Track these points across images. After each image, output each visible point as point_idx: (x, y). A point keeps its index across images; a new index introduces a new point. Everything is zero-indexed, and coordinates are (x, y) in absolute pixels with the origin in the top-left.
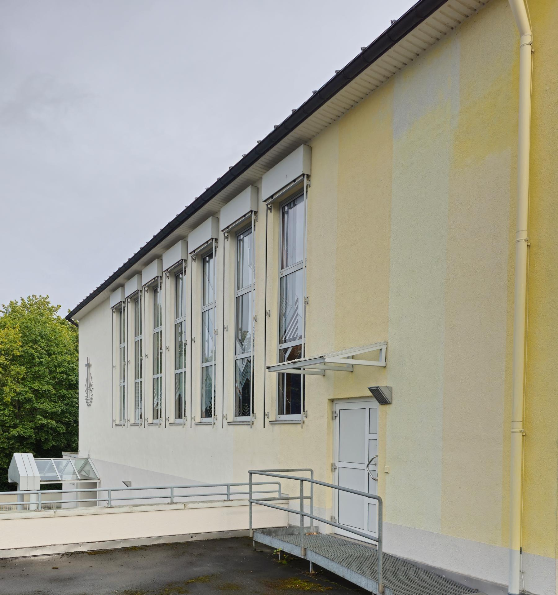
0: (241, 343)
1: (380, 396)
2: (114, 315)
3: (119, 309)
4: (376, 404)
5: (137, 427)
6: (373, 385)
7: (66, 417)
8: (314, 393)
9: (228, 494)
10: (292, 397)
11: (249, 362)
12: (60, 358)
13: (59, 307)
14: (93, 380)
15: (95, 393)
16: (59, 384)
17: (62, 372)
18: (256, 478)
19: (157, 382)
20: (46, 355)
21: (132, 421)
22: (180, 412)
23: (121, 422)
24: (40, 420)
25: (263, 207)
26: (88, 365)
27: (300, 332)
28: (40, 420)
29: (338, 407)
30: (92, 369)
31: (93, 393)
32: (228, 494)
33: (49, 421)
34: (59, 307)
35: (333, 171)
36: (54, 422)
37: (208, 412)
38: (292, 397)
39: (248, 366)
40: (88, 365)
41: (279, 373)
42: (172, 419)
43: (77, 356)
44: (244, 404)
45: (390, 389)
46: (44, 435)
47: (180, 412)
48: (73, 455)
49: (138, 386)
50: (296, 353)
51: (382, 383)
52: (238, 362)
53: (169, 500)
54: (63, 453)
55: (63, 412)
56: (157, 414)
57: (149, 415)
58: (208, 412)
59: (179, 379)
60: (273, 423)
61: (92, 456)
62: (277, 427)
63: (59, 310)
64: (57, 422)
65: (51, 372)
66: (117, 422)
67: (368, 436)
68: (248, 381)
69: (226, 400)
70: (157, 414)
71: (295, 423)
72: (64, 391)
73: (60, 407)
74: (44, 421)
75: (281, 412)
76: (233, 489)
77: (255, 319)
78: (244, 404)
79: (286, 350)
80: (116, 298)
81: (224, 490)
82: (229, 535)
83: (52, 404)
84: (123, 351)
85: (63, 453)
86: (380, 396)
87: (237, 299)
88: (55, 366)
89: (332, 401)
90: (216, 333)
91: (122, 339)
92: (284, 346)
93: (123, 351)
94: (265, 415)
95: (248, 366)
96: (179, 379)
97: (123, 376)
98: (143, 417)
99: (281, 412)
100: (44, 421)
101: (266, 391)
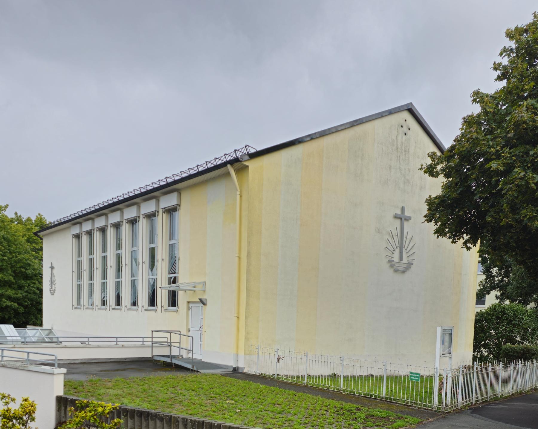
0: (152, 271)
1: (203, 302)
2: (74, 239)
3: (78, 237)
4: (202, 305)
5: (79, 310)
6: (201, 297)
7: (26, 302)
8: (182, 298)
9: (143, 342)
10: (173, 300)
11: (155, 281)
12: (20, 257)
13: (7, 206)
14: (56, 278)
15: (58, 286)
16: (16, 275)
17: (22, 267)
18: (155, 334)
19: (104, 285)
21: (87, 306)
22: (118, 302)
24: (5, 302)
25: (161, 211)
26: (52, 268)
28: (5, 302)
29: (191, 305)
30: (55, 271)
31: (56, 286)
32: (143, 342)
33: (12, 303)
34: (7, 206)
35: (190, 204)
36: (16, 304)
37: (134, 304)
38: (173, 300)
39: (154, 282)
40: (52, 268)
42: (114, 306)
44: (152, 301)
45: (206, 300)
46: (7, 314)
47: (118, 302)
48: (39, 328)
49: (91, 286)
50: (175, 281)
51: (203, 297)
52: (150, 280)
53: (119, 339)
54: (27, 326)
55: (24, 298)
56: (104, 303)
57: (98, 302)
58: (134, 304)
59: (118, 285)
61: (54, 328)
62: (167, 313)
63: (7, 209)
64: (19, 304)
65: (12, 267)
66: (76, 306)
68: (154, 290)
70: (104, 303)
71: (174, 311)
72: (23, 281)
73: (21, 293)
74: (9, 303)
75: (169, 306)
78: (152, 301)
79: (171, 278)
80: (76, 230)
81: (141, 339)
82: (143, 359)
83: (13, 292)
84: (79, 263)
85: (27, 326)
86: (203, 302)
88: (15, 262)
89: (189, 302)
91: (79, 255)
93: (79, 263)
94: (162, 307)
95: (154, 282)
96: (118, 285)
97: (79, 277)
98: (94, 304)
99: (169, 306)
100: (9, 303)
101: (162, 297)
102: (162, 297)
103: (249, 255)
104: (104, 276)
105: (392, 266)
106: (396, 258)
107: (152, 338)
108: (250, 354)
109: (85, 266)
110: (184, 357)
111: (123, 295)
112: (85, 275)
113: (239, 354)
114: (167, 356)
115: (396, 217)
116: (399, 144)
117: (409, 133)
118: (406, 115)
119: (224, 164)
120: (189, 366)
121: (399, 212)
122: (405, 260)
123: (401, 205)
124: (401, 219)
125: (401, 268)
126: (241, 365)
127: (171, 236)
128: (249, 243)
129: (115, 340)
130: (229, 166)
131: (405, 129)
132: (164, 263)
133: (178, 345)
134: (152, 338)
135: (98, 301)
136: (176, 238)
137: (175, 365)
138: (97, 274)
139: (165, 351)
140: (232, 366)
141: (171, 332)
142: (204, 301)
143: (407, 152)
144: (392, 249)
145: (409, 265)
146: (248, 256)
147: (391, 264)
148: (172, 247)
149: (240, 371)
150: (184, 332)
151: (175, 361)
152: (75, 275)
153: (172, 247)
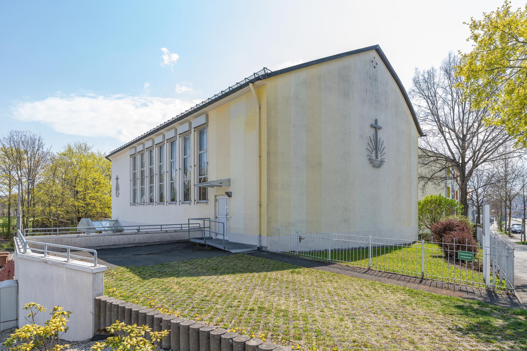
1: (229, 195)
4: (228, 197)
8: (211, 193)
15: (121, 191)
20: (458, 137)
23: (134, 202)
27: (206, 173)
30: (119, 180)
41: (200, 188)
43: (299, 252)
51: (229, 190)
60: (198, 203)
67: (226, 207)
69: (180, 195)
76: (183, 226)
77: (191, 167)
81: (180, 226)
87: (184, 159)
90: (176, 170)
92: (201, 177)
93: (134, 174)
95: (188, 183)
97: (135, 184)
99: (200, 199)
101: (194, 193)
102: (194, 193)
103: (268, 153)
104: (151, 182)
105: (371, 163)
106: (374, 157)
107: (189, 224)
108: (271, 236)
109: (138, 176)
110: (214, 238)
111: (165, 194)
112: (139, 182)
113: (262, 235)
114: (202, 239)
115: (372, 126)
116: (371, 74)
117: (377, 66)
118: (374, 53)
119: (247, 84)
120: (221, 247)
121: (373, 123)
122: (379, 159)
123: (374, 119)
124: (376, 128)
125: (377, 163)
126: (264, 244)
127: (201, 147)
128: (268, 144)
129: (160, 227)
130: (250, 84)
131: (374, 63)
132: (196, 168)
133: (208, 229)
134: (189, 224)
135: (147, 197)
136: (205, 148)
137: (209, 246)
138: (147, 181)
139: (199, 235)
140: (256, 246)
141: (204, 219)
142: (230, 194)
143: (376, 80)
144: (371, 150)
145: (382, 162)
146: (267, 155)
147: (371, 160)
148: (200, 157)
149: (263, 249)
150: (212, 218)
151: (208, 243)
152: (132, 182)
153: (200, 157)
